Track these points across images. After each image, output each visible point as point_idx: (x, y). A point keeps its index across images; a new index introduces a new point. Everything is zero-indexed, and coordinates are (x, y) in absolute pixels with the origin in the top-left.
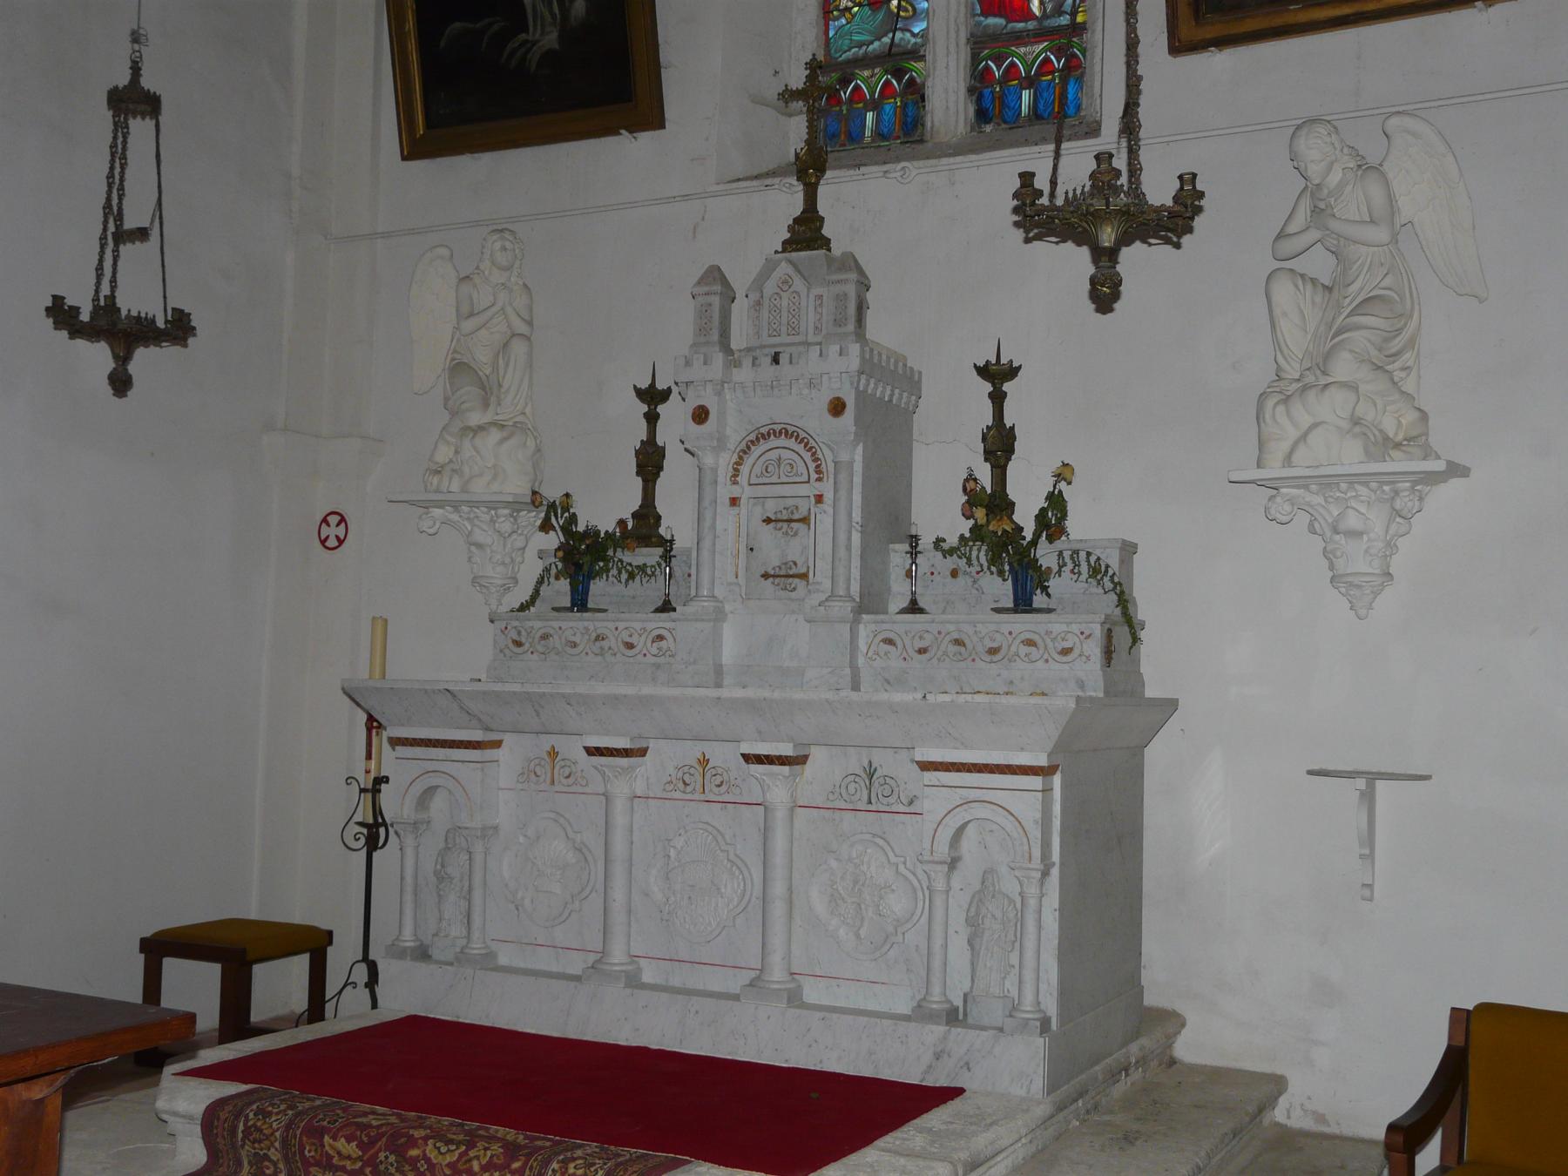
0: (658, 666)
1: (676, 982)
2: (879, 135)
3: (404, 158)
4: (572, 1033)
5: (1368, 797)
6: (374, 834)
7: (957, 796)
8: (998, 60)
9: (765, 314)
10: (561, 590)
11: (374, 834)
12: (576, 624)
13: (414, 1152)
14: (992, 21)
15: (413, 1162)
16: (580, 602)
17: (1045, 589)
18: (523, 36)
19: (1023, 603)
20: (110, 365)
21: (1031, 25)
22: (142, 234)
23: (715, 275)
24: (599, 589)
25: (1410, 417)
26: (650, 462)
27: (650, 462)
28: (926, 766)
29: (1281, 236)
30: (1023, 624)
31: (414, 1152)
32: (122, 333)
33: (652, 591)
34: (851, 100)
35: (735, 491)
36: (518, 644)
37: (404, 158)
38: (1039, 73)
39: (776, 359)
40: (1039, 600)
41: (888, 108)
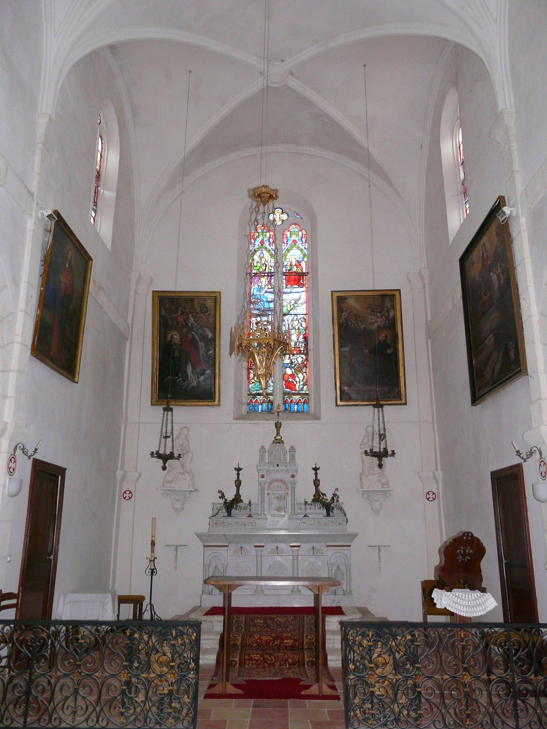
0: (252, 529)
1: (276, 594)
2: (262, 411)
3: (152, 405)
4: (252, 606)
5: (379, 550)
6: (153, 572)
7: (334, 551)
8: (289, 398)
9: (273, 456)
10: (224, 512)
11: (153, 572)
12: (230, 520)
13: (275, 620)
14: (287, 390)
15: (276, 622)
16: (229, 515)
17: (332, 512)
18: (187, 382)
19: (328, 515)
20: (162, 464)
21: (296, 392)
22: (169, 437)
23: (263, 448)
24: (233, 511)
25: (385, 480)
26: (238, 484)
27: (238, 484)
28: (328, 546)
29: (361, 444)
30: (329, 519)
31: (275, 620)
32: (165, 458)
33: (247, 512)
34: (255, 402)
35: (269, 492)
36: (216, 524)
37: (152, 405)
38: (298, 402)
39: (278, 465)
40: (331, 514)
41: (264, 405)
